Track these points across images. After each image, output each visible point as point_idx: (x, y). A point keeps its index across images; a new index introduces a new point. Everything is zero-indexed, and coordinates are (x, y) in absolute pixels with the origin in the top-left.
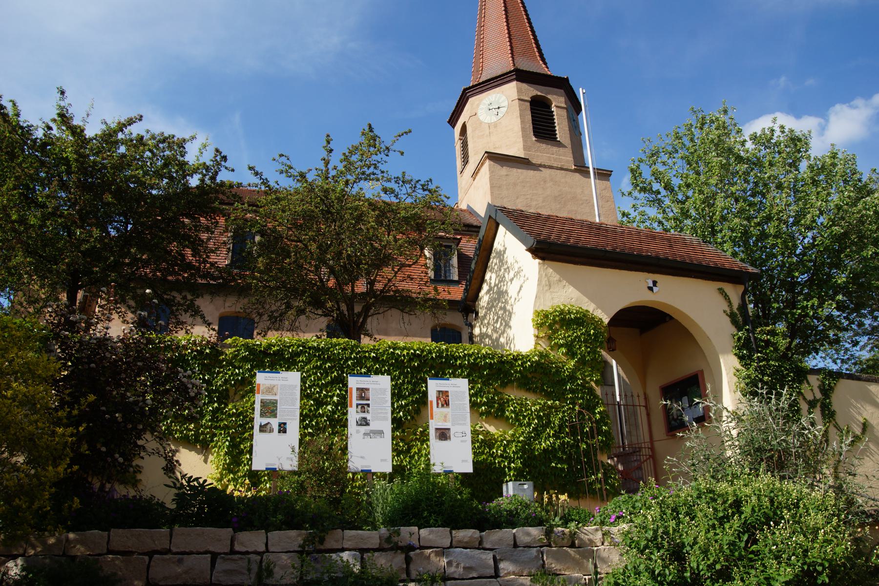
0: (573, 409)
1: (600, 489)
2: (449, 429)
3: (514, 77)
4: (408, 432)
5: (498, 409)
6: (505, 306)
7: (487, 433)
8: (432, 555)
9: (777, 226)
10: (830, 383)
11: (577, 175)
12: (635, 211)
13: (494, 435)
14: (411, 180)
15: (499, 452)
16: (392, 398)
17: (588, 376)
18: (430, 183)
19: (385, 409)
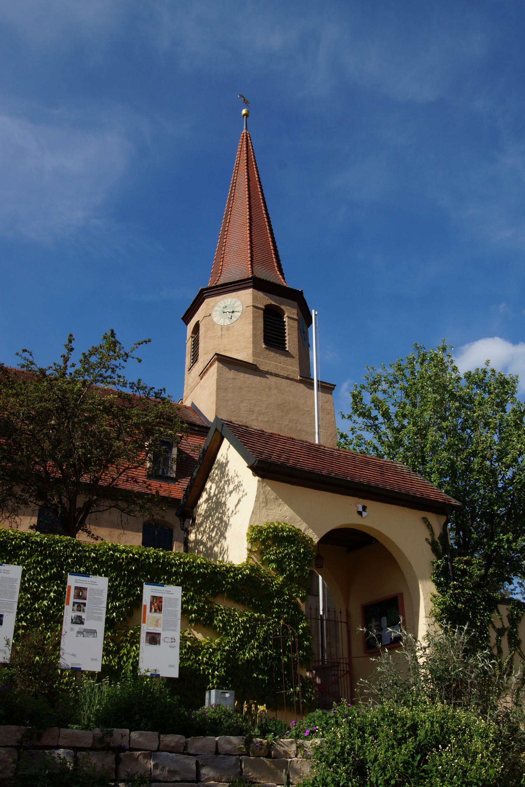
0: (278, 623)
1: (298, 702)
2: (159, 634)
3: (251, 284)
4: (119, 633)
5: (207, 618)
6: (222, 517)
7: (195, 640)
8: (141, 757)
9: (481, 463)
10: (518, 613)
11: (302, 386)
12: (353, 434)
13: (201, 642)
14: (146, 387)
15: (205, 659)
16: (108, 599)
17: (294, 592)
18: (163, 392)
19: (100, 610)
